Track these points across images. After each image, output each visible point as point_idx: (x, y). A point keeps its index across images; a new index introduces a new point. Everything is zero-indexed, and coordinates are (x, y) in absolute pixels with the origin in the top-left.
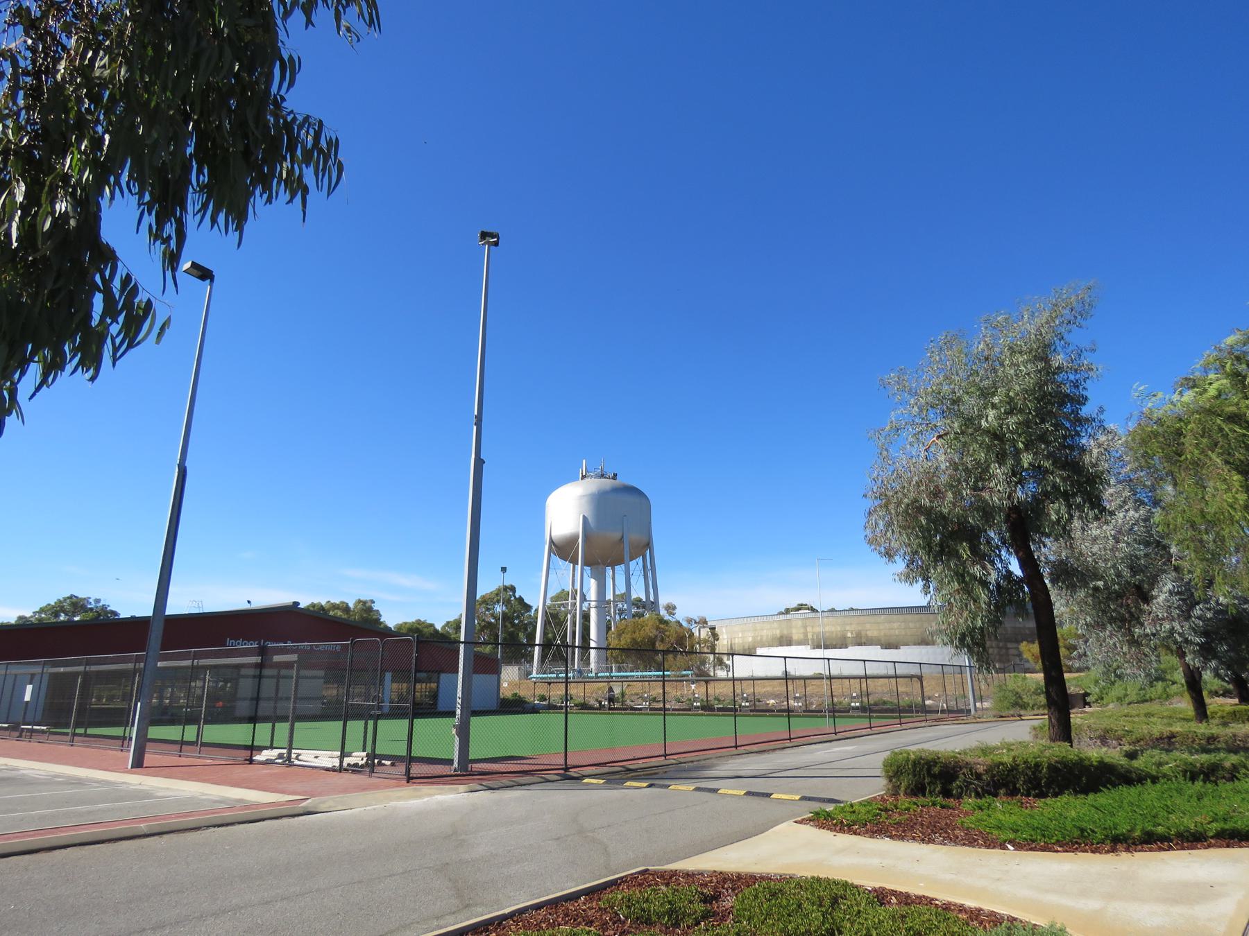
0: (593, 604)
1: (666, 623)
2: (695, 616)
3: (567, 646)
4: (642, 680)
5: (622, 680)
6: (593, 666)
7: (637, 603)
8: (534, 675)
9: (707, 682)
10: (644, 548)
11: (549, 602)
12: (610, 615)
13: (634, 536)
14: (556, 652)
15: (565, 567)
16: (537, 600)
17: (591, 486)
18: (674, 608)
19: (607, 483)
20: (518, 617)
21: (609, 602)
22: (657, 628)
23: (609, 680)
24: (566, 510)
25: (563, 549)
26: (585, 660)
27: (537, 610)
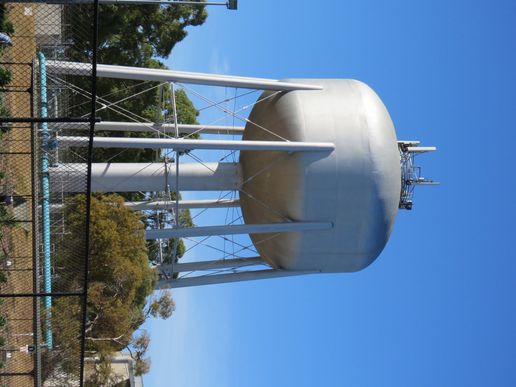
0: (172, 168)
1: (140, 301)
2: (151, 354)
3: (92, 121)
4: (37, 255)
5: (36, 222)
6: (61, 168)
7: (175, 249)
8: (46, 63)
9: (33, 374)
10: (274, 260)
11: (175, 87)
12: (153, 198)
13: (296, 240)
14: (86, 100)
15: (237, 113)
16: (175, 68)
17: (389, 163)
18: (165, 315)
19: (392, 191)
20: (147, 31)
21: (175, 196)
22: (128, 285)
23: (37, 198)
24: (343, 115)
25: (270, 112)
26: (72, 155)
27: (160, 66)
